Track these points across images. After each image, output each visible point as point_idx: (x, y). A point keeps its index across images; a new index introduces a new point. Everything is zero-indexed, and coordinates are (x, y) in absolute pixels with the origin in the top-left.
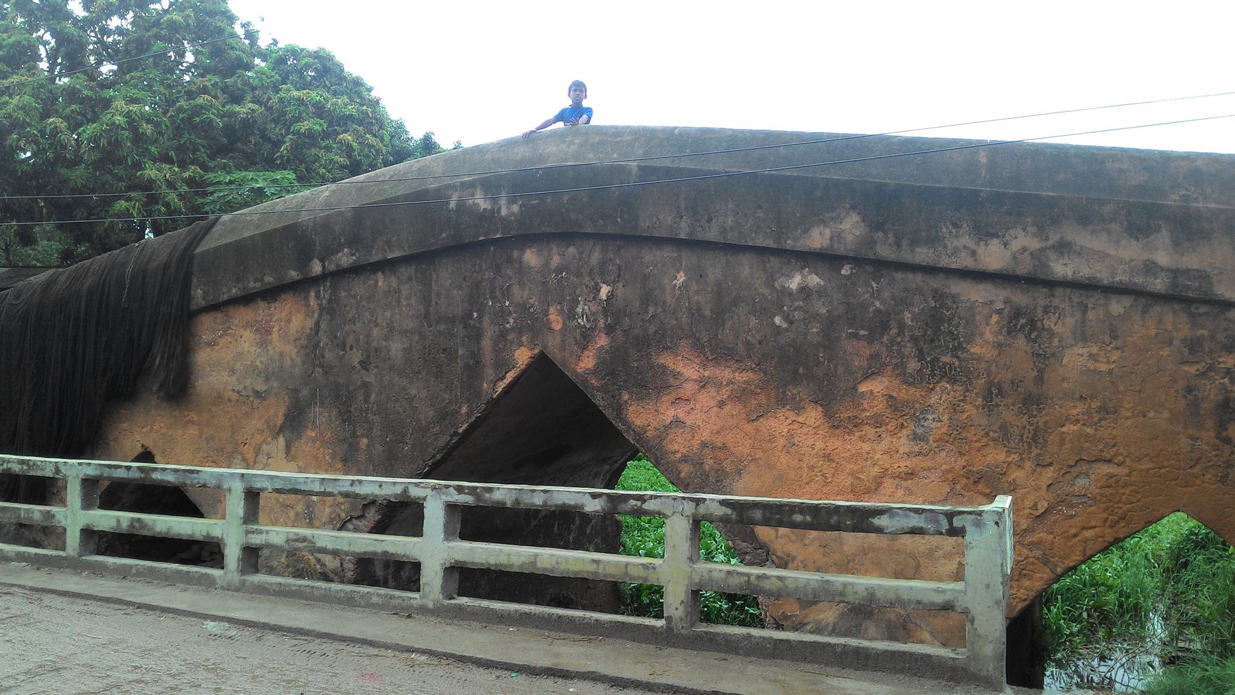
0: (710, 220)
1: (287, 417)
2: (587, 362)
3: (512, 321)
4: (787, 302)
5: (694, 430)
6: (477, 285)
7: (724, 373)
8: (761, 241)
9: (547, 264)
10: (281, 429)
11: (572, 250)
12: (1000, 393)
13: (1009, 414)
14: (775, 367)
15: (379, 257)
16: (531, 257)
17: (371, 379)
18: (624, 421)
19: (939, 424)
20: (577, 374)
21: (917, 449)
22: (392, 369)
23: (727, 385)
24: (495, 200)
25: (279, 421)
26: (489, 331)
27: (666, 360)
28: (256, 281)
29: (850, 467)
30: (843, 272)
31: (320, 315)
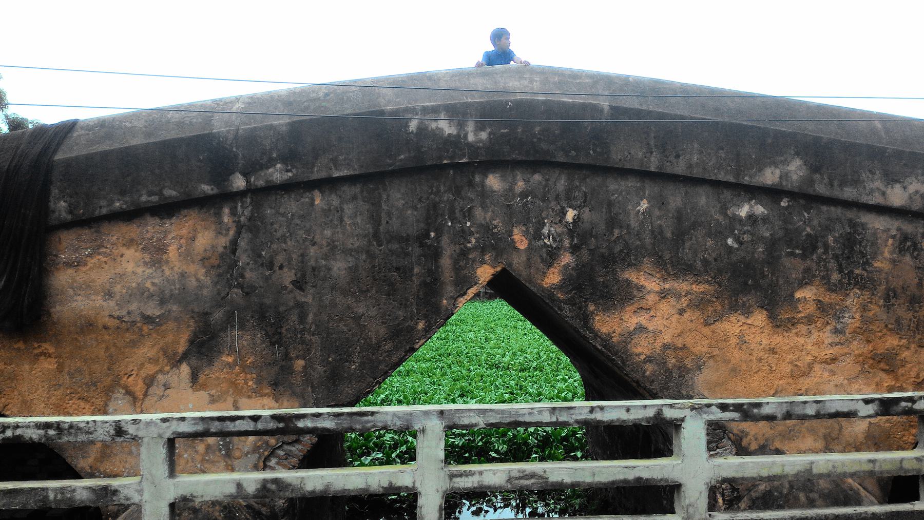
0: (678, 156)
1: (192, 342)
2: (553, 278)
4: (738, 226)
5: (656, 333)
6: (435, 206)
7: (683, 286)
8: (721, 177)
9: (511, 189)
10: (185, 357)
11: (537, 177)
12: (895, 296)
13: (902, 311)
14: (729, 280)
15: (323, 175)
16: (494, 182)
17: (308, 298)
18: (592, 330)
19: (852, 321)
20: (543, 289)
21: (837, 340)
22: (333, 288)
23: (686, 295)
24: (461, 125)
25: (181, 348)
27: (631, 275)
28: (150, 194)
29: (789, 357)
30: (782, 204)
31: (238, 233)
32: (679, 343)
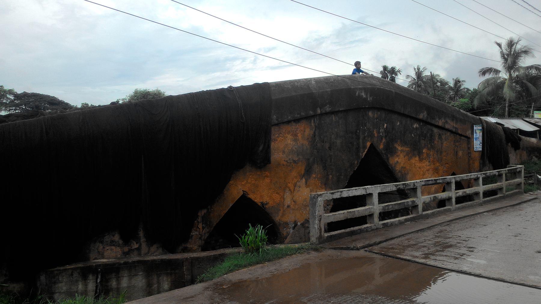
10: (304, 176)
11: (379, 113)
16: (370, 114)
25: (303, 172)
26: (362, 137)
28: (298, 114)
31: (316, 130)
32: (404, 166)
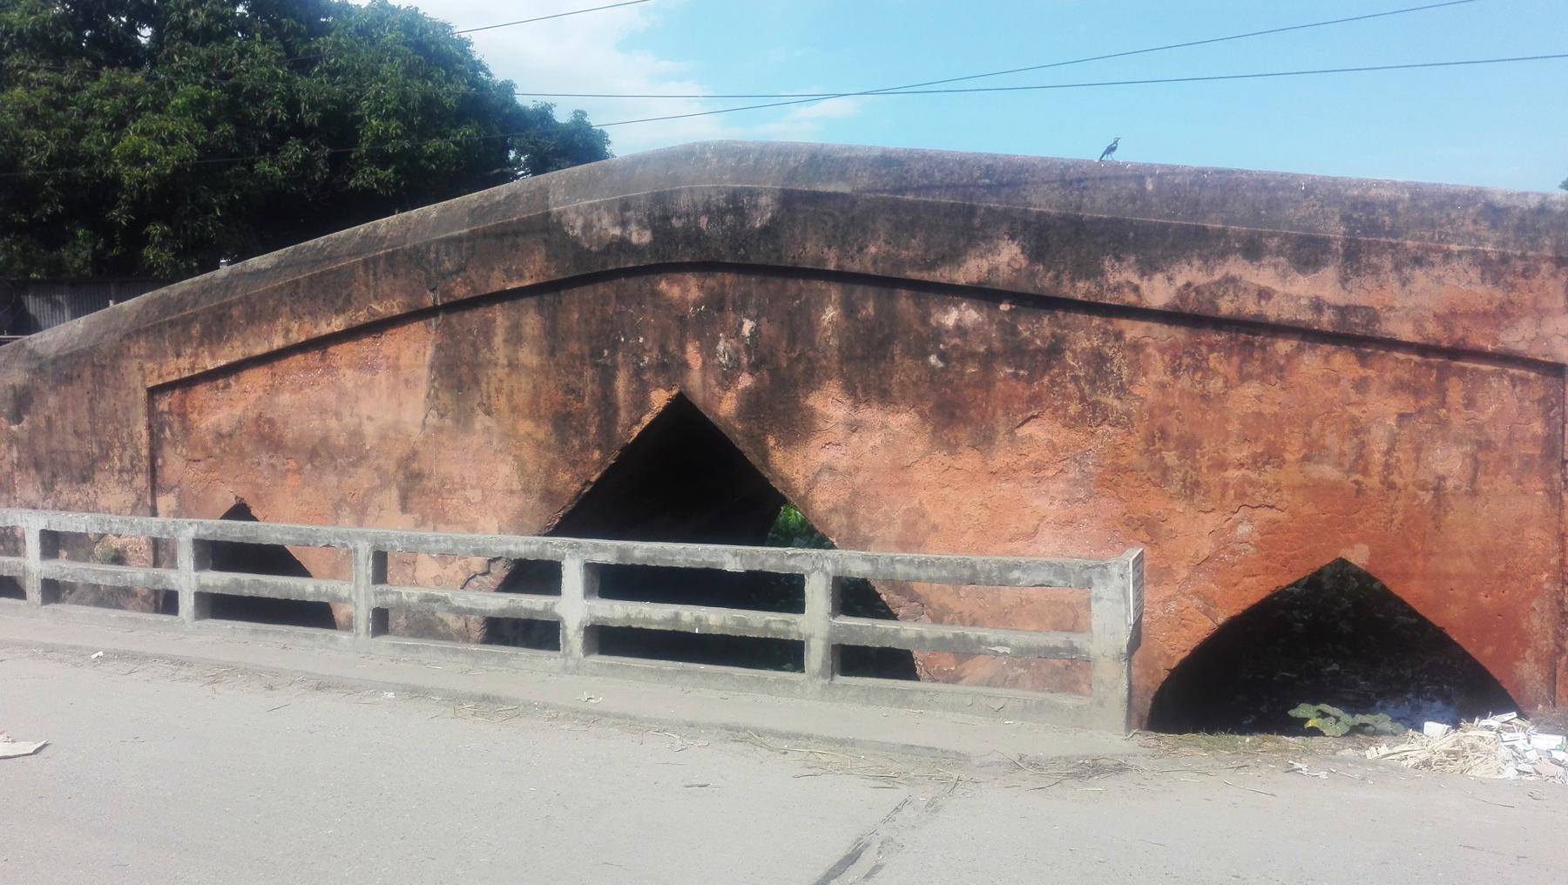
3: (646, 359)
